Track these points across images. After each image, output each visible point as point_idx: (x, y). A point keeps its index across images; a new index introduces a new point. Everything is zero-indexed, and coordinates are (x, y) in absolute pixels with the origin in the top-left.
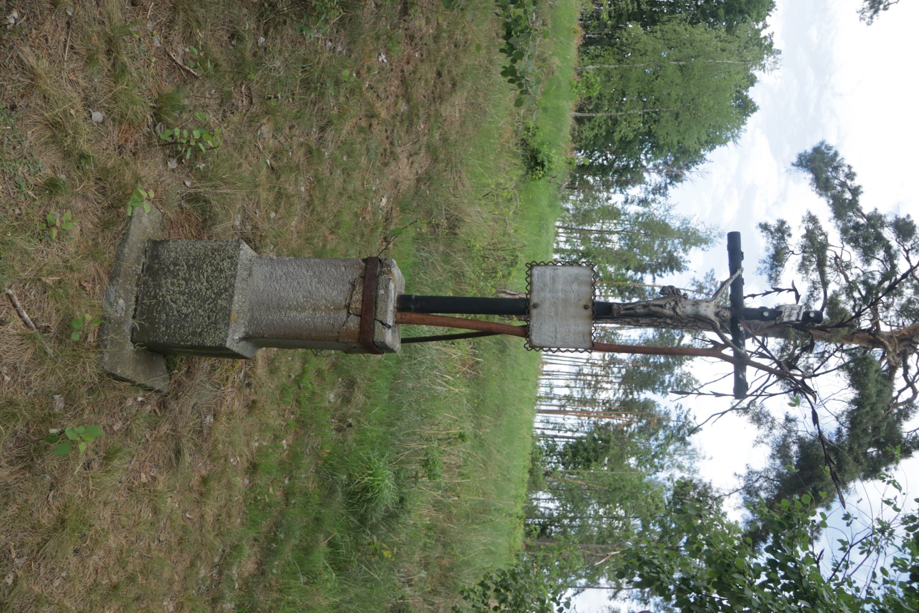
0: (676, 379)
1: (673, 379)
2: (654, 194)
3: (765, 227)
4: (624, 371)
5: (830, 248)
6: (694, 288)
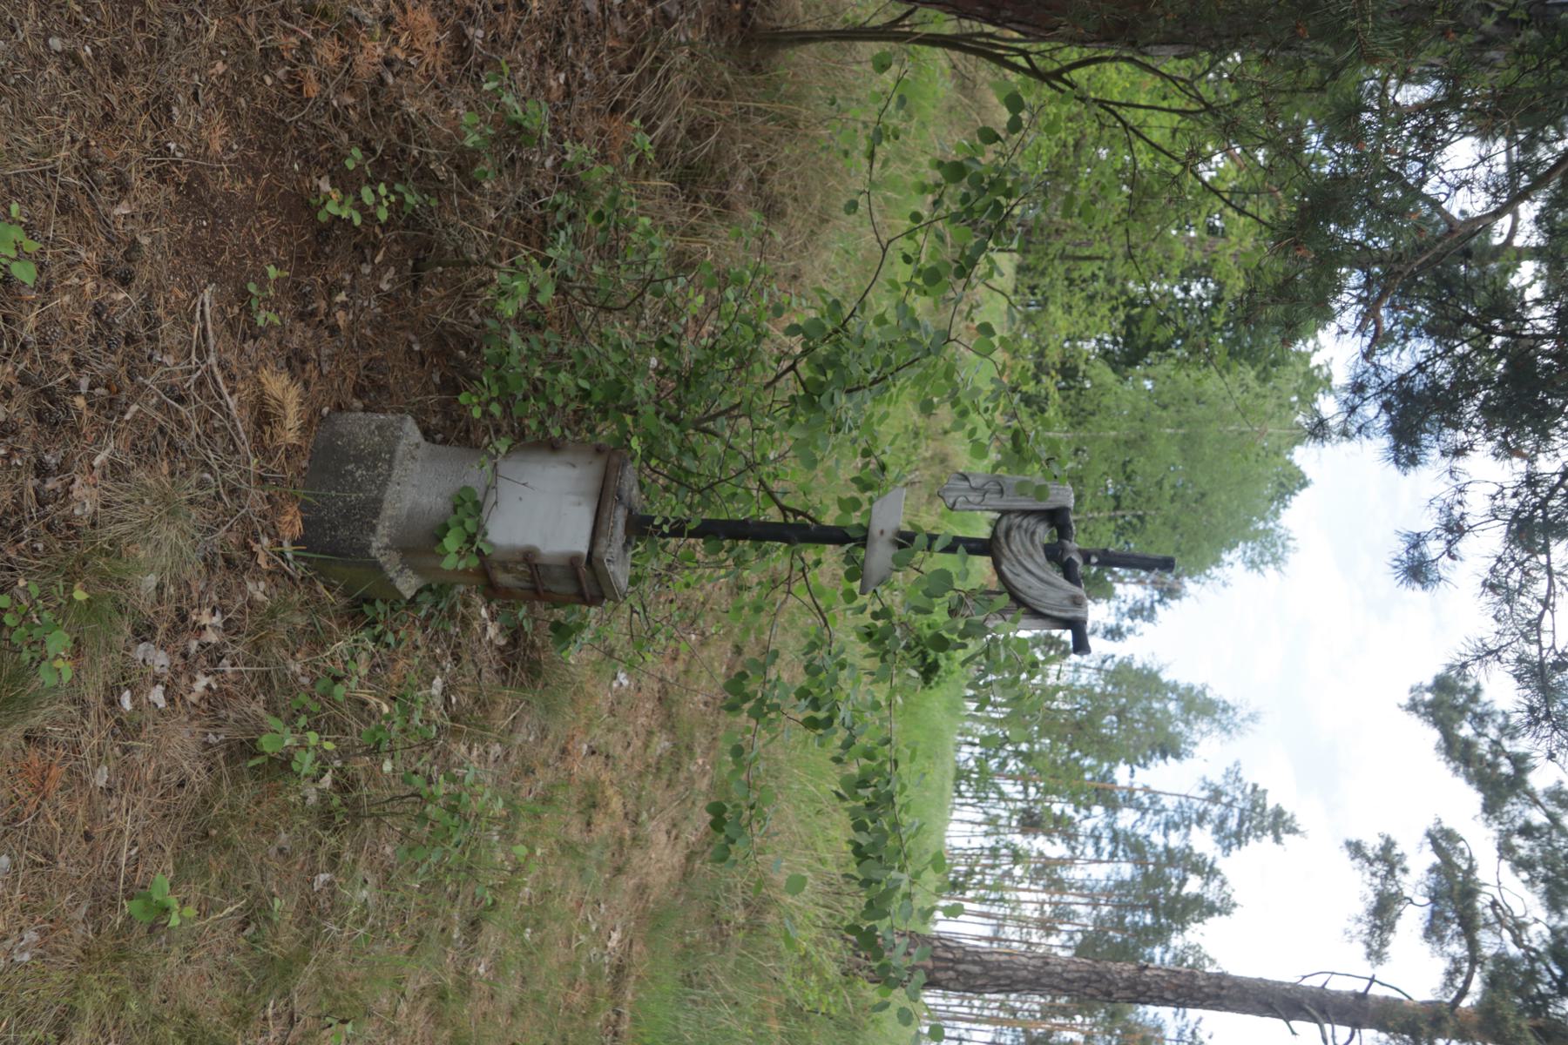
0: (1175, 956)
1: (1168, 957)
2: (1132, 618)
3: (1356, 849)
4: (1078, 937)
5: (1484, 889)
6: (1205, 794)
